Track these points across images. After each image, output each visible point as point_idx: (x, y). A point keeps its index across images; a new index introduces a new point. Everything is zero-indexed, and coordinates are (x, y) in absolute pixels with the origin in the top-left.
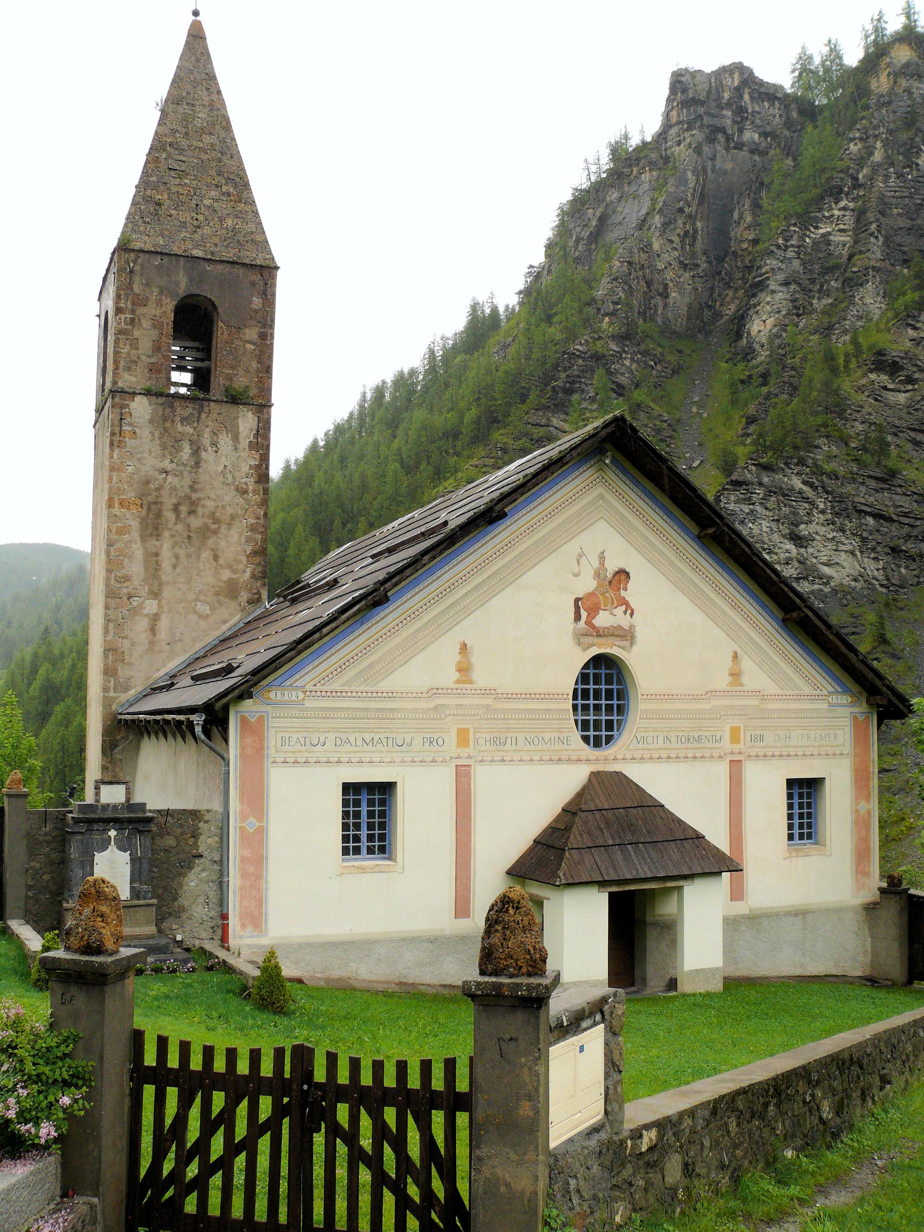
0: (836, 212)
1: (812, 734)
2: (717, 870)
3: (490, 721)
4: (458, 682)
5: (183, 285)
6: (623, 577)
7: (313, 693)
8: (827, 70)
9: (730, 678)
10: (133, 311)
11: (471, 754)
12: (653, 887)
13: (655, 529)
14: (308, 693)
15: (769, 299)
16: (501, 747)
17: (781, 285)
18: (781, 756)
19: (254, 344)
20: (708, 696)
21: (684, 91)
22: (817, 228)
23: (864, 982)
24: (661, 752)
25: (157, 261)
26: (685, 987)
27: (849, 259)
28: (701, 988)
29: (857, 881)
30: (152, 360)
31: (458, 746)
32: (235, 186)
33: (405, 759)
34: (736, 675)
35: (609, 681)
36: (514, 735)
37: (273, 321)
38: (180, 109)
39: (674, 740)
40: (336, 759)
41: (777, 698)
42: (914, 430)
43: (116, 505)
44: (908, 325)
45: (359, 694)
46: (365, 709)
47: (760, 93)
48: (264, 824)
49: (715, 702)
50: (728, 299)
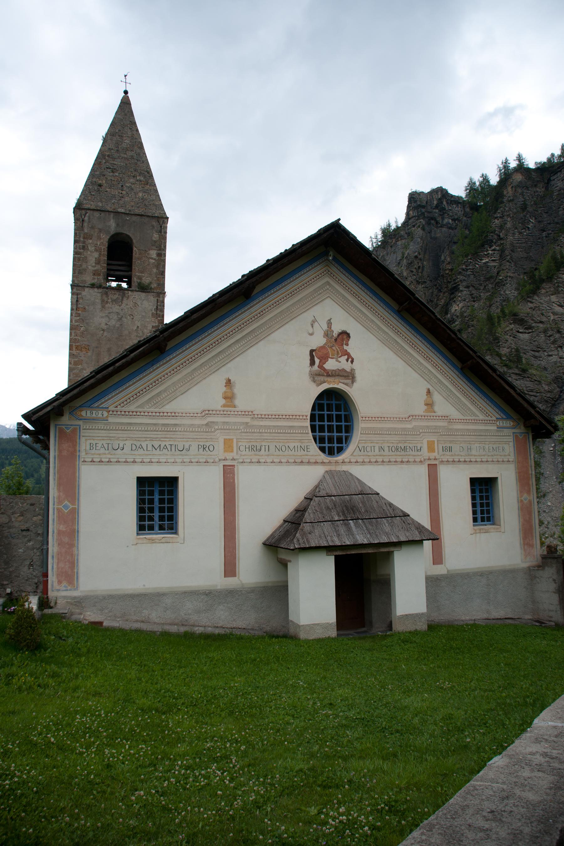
0: (490, 252)
1: (487, 447)
2: (418, 539)
3: (249, 434)
4: (224, 406)
5: (112, 226)
6: (345, 337)
7: (115, 413)
8: (482, 188)
9: (426, 407)
10: (84, 242)
11: (235, 457)
12: (370, 552)
13: (367, 305)
14: (111, 413)
15: (460, 294)
16: (257, 453)
17: (465, 287)
18: (465, 461)
19: (154, 259)
20: (410, 419)
21: (415, 202)
22: (481, 260)
23: (535, 623)
24: (377, 457)
25: (97, 214)
26: (398, 627)
27: (498, 274)
28: (410, 627)
29: (525, 550)
30: (95, 269)
31: (225, 451)
32: (145, 177)
33: (185, 460)
34: (430, 405)
35: (338, 408)
36: (267, 444)
37: (165, 247)
38: (115, 139)
39: (386, 449)
40: (132, 460)
41: (460, 421)
42: (534, 351)
43: (74, 349)
44: (528, 301)
45: (150, 414)
46: (155, 424)
47: (451, 201)
48: (76, 507)
49: (414, 423)
50: (440, 297)
